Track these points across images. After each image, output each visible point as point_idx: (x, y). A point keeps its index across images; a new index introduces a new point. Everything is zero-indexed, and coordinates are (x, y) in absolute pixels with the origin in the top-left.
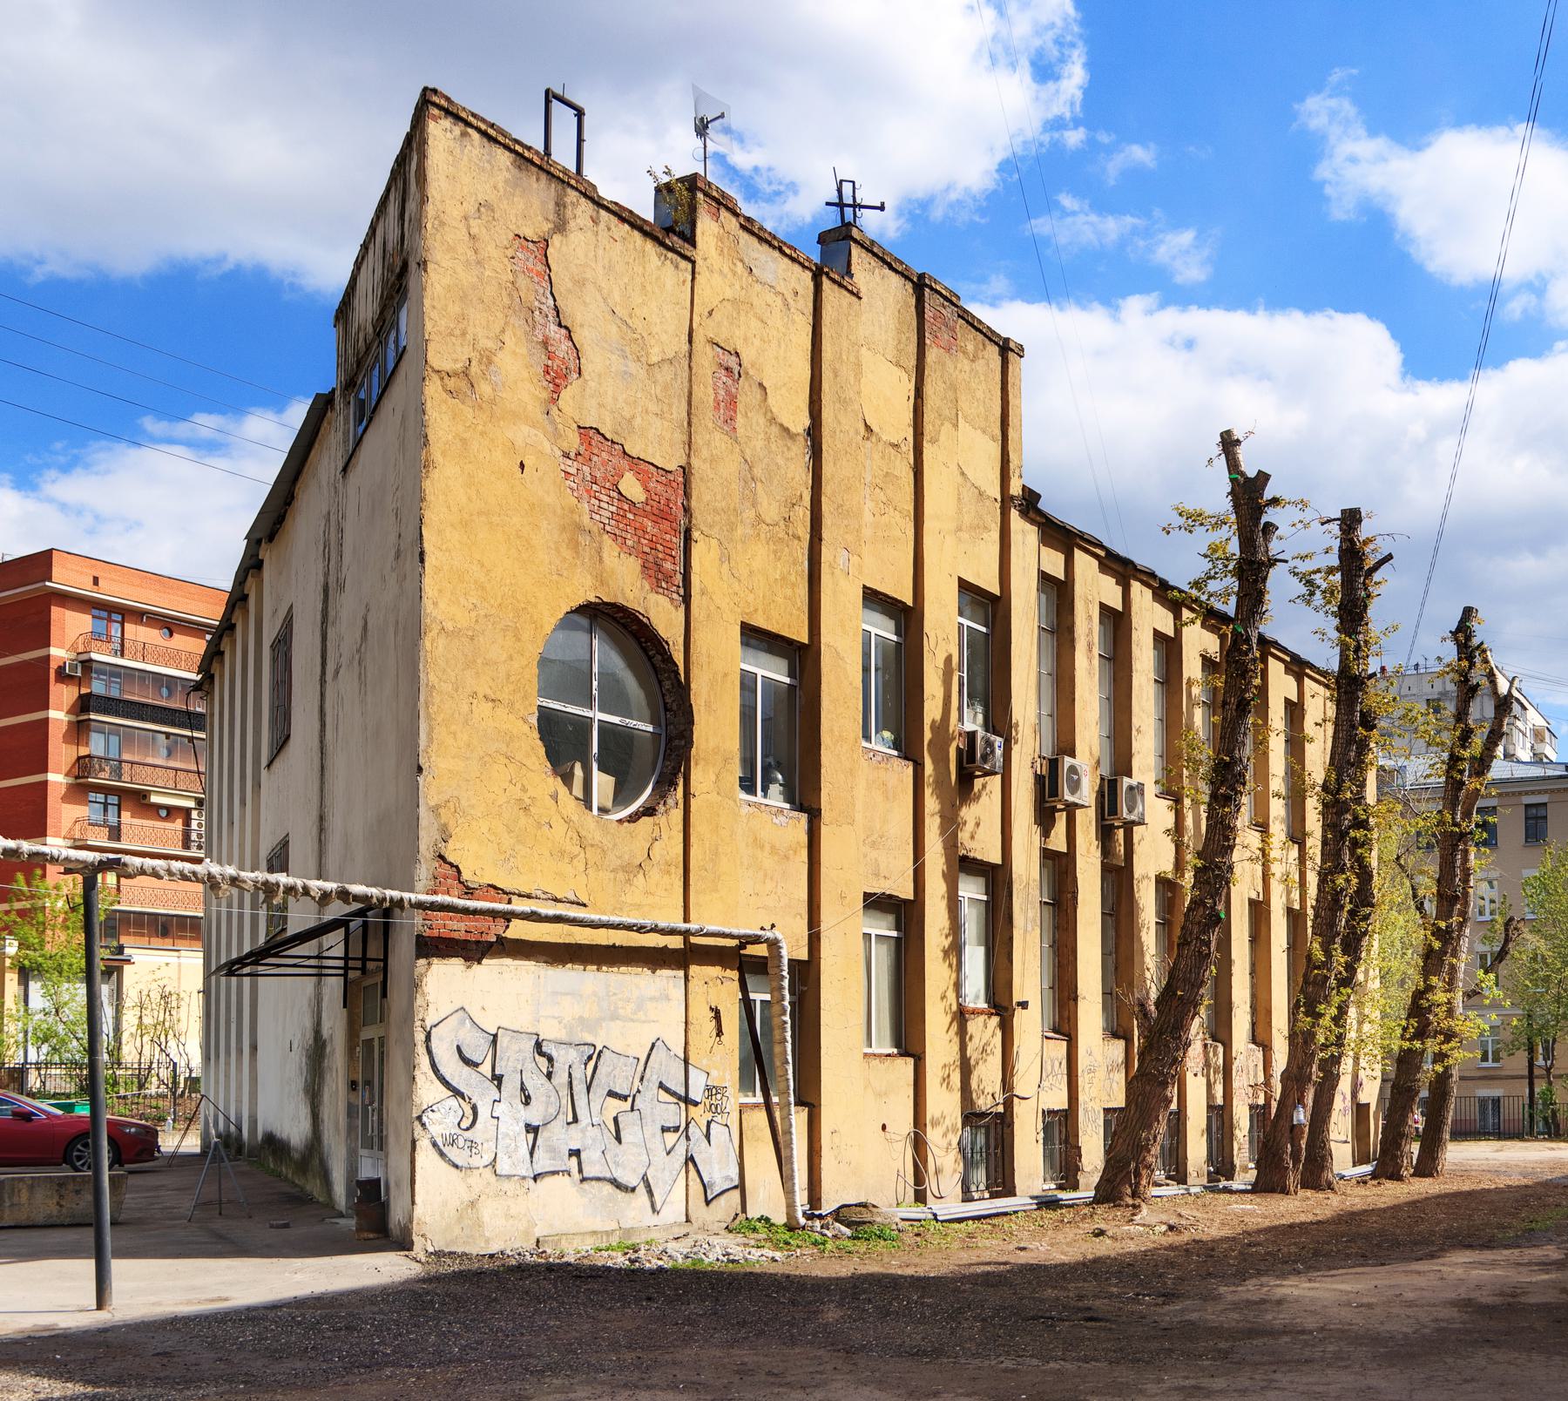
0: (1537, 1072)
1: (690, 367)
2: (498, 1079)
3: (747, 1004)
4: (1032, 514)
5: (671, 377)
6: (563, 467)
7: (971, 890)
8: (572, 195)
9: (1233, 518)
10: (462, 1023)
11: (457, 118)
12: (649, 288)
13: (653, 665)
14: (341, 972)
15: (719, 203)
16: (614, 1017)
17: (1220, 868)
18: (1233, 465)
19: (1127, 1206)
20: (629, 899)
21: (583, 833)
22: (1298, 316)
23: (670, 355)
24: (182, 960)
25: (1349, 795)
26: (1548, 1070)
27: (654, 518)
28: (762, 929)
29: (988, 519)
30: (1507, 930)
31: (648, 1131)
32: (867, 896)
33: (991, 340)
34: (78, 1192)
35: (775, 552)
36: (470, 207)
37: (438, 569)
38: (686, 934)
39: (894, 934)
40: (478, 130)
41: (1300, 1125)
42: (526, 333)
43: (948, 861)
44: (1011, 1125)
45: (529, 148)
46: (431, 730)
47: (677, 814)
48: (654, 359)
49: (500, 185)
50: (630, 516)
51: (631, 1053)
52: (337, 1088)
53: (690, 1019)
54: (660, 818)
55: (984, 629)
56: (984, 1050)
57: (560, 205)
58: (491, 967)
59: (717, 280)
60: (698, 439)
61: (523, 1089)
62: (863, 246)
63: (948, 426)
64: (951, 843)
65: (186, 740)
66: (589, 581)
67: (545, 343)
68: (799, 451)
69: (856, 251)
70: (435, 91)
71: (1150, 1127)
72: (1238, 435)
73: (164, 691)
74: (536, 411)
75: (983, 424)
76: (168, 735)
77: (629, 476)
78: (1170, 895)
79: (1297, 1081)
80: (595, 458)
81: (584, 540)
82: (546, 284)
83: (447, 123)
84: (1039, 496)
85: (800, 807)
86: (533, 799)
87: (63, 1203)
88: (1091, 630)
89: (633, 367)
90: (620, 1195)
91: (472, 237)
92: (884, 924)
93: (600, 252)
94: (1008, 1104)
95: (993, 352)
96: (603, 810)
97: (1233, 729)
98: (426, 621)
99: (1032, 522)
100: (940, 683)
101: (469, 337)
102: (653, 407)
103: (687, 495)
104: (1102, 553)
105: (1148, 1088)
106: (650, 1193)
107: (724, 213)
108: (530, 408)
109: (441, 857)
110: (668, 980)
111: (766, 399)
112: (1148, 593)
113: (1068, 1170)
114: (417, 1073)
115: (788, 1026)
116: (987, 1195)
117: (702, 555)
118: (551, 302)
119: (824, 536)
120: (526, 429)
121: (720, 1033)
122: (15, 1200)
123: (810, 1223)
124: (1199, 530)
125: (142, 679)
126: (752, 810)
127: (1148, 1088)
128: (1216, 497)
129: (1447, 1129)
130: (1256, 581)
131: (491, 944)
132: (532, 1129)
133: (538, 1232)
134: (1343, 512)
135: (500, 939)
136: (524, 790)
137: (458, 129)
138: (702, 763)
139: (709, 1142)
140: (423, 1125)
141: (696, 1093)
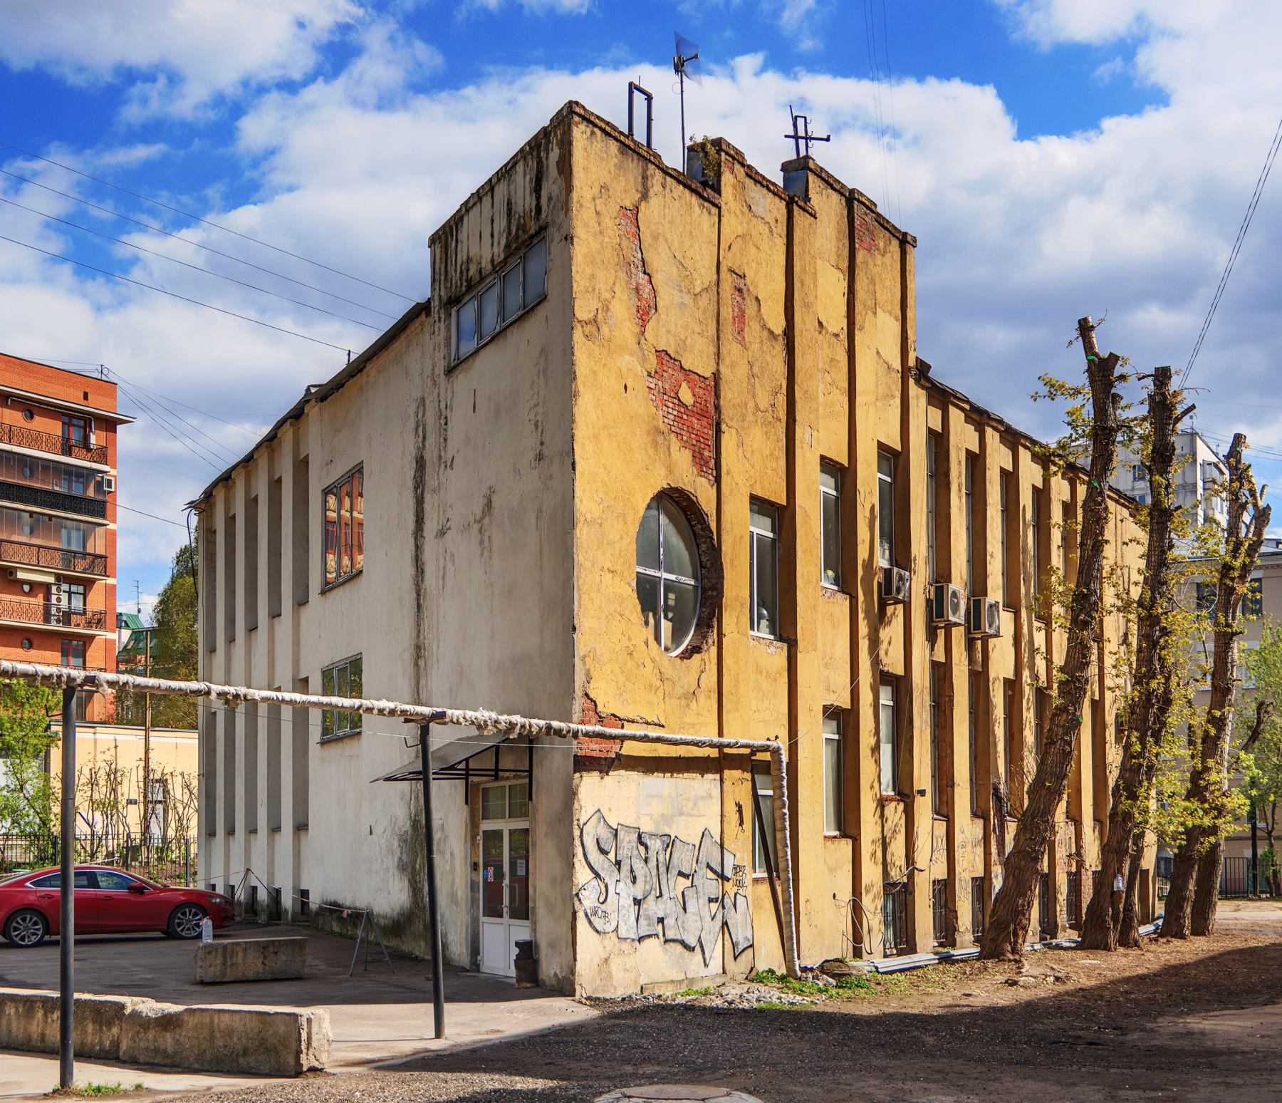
0: (1259, 833)
1: (718, 293)
2: (618, 863)
3: (756, 797)
4: (923, 382)
5: (706, 301)
6: (647, 384)
7: (886, 698)
8: (651, 167)
9: (1088, 389)
10: (599, 821)
11: (589, 121)
12: (694, 233)
13: (694, 532)
15: (734, 158)
16: (681, 813)
17: (1079, 681)
18: (1089, 347)
19: (1010, 961)
20: (687, 720)
21: (662, 670)
22: (1055, 137)
23: (706, 286)
24: (98, 736)
25: (1160, 611)
26: (1269, 833)
27: (698, 417)
28: (768, 739)
29: (894, 387)
30: (1259, 713)
31: (701, 901)
32: (826, 708)
33: (894, 236)
34: (276, 953)
35: (766, 433)
36: (596, 190)
37: (583, 474)
38: (720, 747)
39: (836, 737)
40: (600, 128)
41: (1119, 892)
42: (627, 283)
43: (874, 676)
44: (912, 893)
46: (580, 596)
47: (714, 650)
49: (612, 169)
50: (685, 417)
51: (691, 841)
52: (453, 868)
53: (725, 813)
54: (704, 655)
55: (888, 479)
56: (895, 831)
58: (616, 776)
59: (733, 220)
60: (724, 351)
61: (632, 871)
62: (815, 174)
63: (870, 313)
64: (876, 662)
65: (47, 518)
66: (663, 472)
67: (637, 290)
68: (779, 348)
69: (811, 178)
70: (577, 103)
71: (1025, 895)
72: (1091, 321)
73: (27, 471)
74: (632, 341)
75: (890, 308)
76: (31, 514)
77: (684, 385)
78: (1010, 693)
79: (1117, 853)
80: (665, 374)
81: (660, 439)
82: (637, 242)
83: (583, 127)
84: (929, 367)
85: (780, 638)
87: (266, 962)
88: (960, 473)
90: (686, 953)
91: (597, 213)
92: (829, 729)
93: (667, 210)
94: (911, 876)
95: (895, 243)
96: (667, 649)
97: (1089, 566)
98: (577, 515)
99: (923, 387)
100: (867, 529)
101: (597, 291)
102: (697, 329)
103: (717, 396)
104: (967, 407)
105: (1023, 863)
106: (703, 951)
108: (629, 341)
109: (587, 695)
110: (709, 782)
112: (997, 435)
113: (947, 930)
114: (575, 860)
115: (787, 817)
116: (895, 952)
117: (728, 441)
118: (640, 255)
119: (797, 418)
120: (627, 358)
121: (741, 823)
122: (234, 960)
123: (804, 975)
124: (1060, 399)
125: (8, 460)
126: (755, 642)
127: (1023, 863)
128: (1074, 370)
129: (1216, 892)
130: (1107, 444)
131: (613, 760)
132: (637, 902)
133: (642, 981)
134: (1157, 369)
135: (619, 756)
136: (630, 639)
138: (729, 609)
140: (580, 900)
141: (728, 872)
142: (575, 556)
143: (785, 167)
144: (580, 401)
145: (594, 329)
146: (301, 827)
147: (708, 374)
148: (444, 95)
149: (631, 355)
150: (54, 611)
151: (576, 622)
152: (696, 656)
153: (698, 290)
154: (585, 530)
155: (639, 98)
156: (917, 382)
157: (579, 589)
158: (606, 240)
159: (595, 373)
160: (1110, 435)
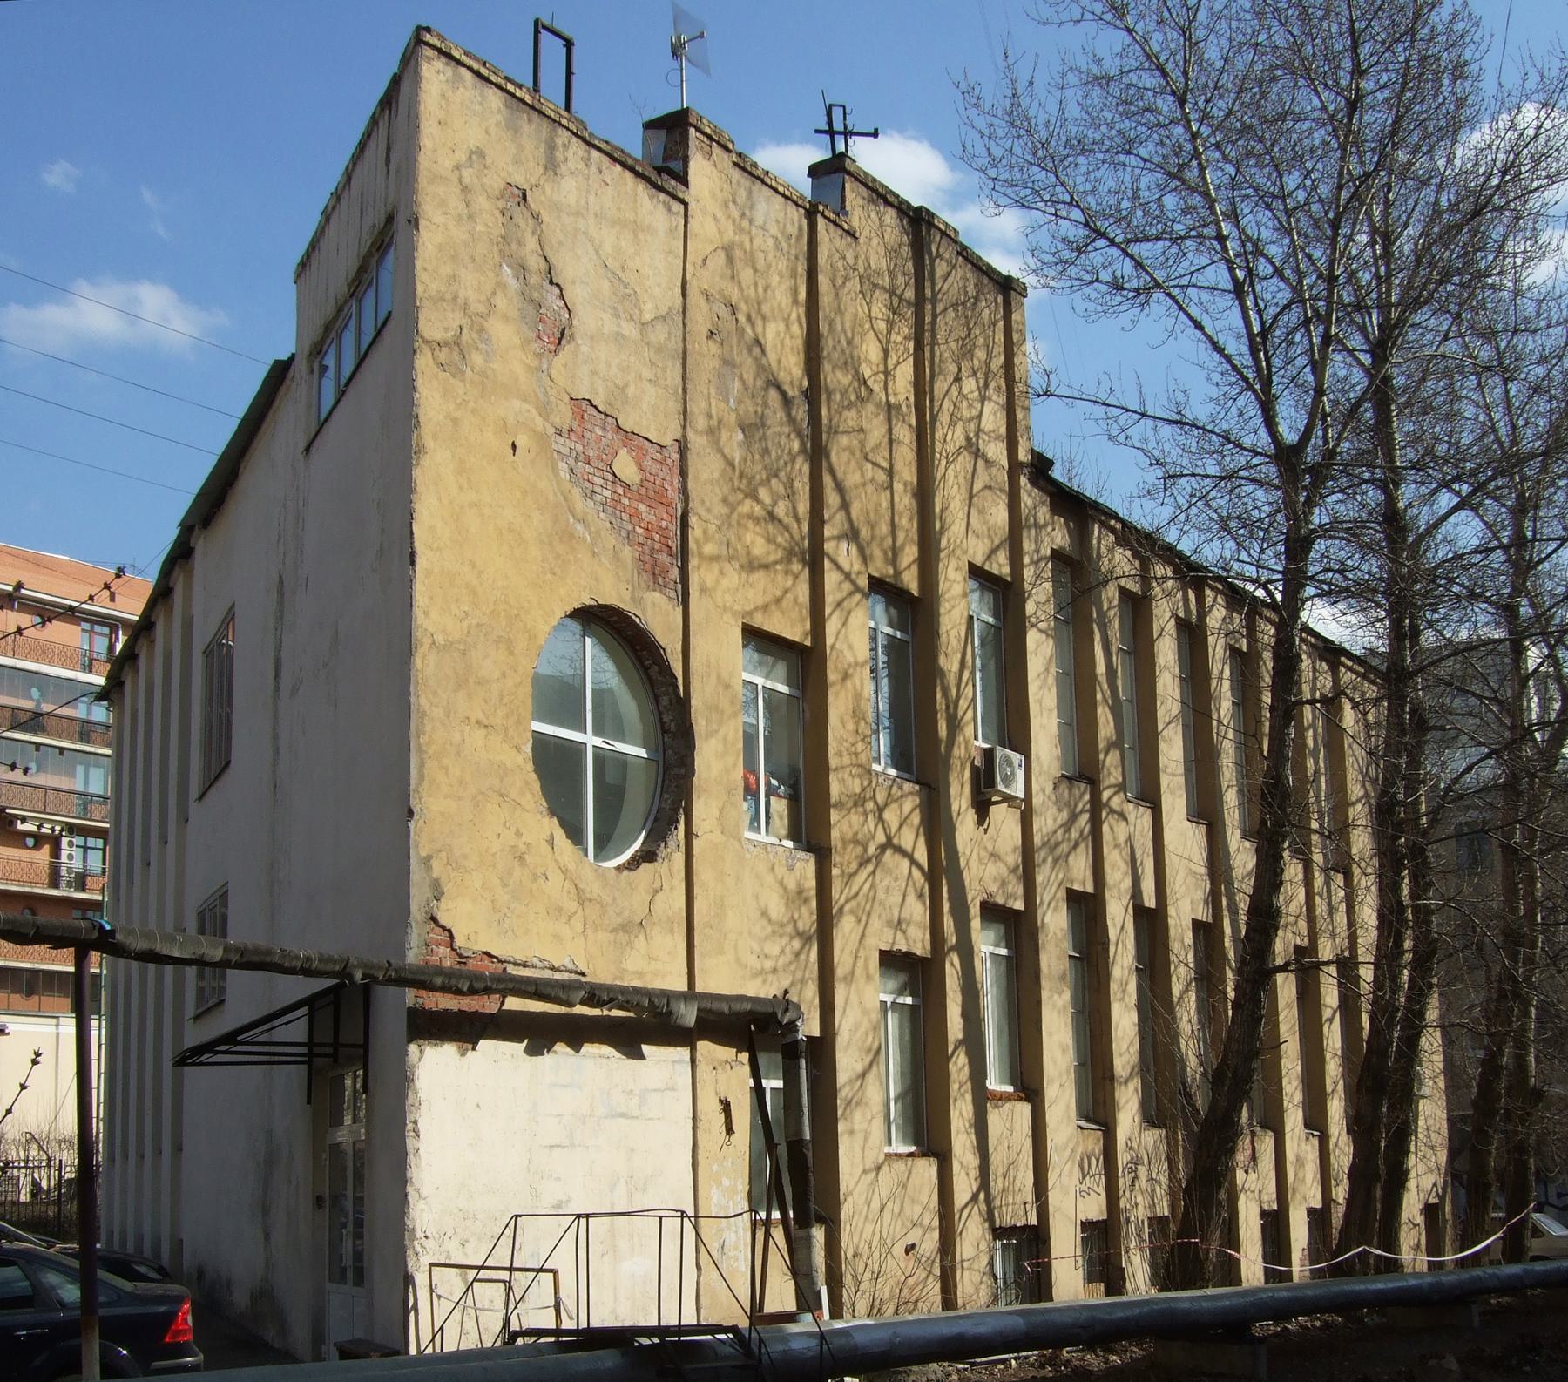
1: (684, 325)
21: (581, 886)
37: (429, 573)
40: (470, 69)
46: (422, 766)
47: (679, 858)
54: (659, 867)
70: (428, 30)
77: (623, 453)
80: (588, 435)
83: (439, 64)
86: (528, 845)
93: (592, 198)
98: (418, 634)
103: (683, 473)
107: (717, 150)
109: (434, 919)
120: (517, 404)
121: (730, 1131)
136: (518, 834)
142: (413, 699)
143: (815, 171)
144: (426, 461)
145: (456, 357)
146: (178, 1148)
147: (667, 440)
149: (525, 401)
150: (64, 871)
151: (413, 803)
152: (645, 866)
153: (648, 317)
154: (432, 658)
155: (552, 48)
156: (1034, 482)
157: (420, 750)
158: (479, 228)
159: (455, 421)
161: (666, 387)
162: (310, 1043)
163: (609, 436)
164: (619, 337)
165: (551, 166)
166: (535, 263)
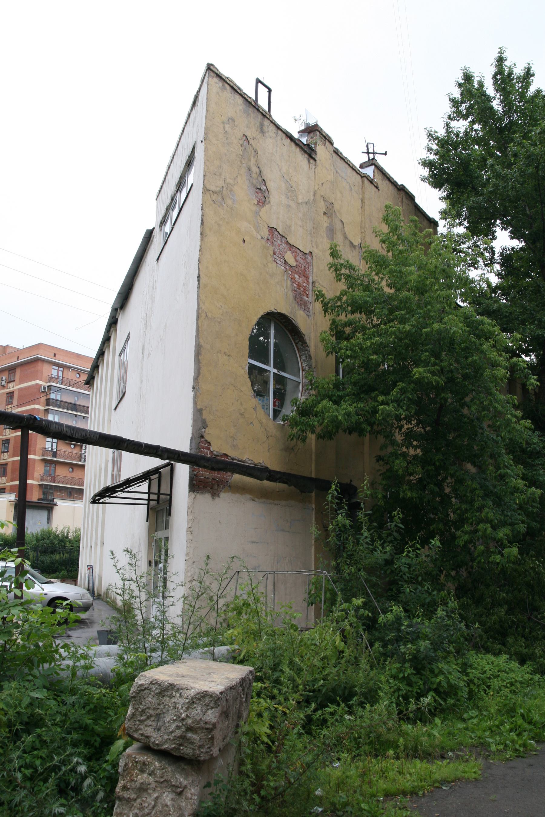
8: (266, 122)
14: (146, 502)
45: (250, 98)
48: (300, 201)
57: (262, 126)
70: (212, 65)
77: (289, 253)
86: (245, 409)
89: (292, 204)
93: (278, 149)
101: (223, 177)
107: (327, 143)
111: (344, 227)
137: (220, 84)
139: (194, 148)
145: (220, 199)
148: (237, 495)
160: (508, 273)
161: (307, 230)
162: (149, 493)
163: (283, 245)
164: (288, 206)
165: (262, 131)
166: (254, 169)
